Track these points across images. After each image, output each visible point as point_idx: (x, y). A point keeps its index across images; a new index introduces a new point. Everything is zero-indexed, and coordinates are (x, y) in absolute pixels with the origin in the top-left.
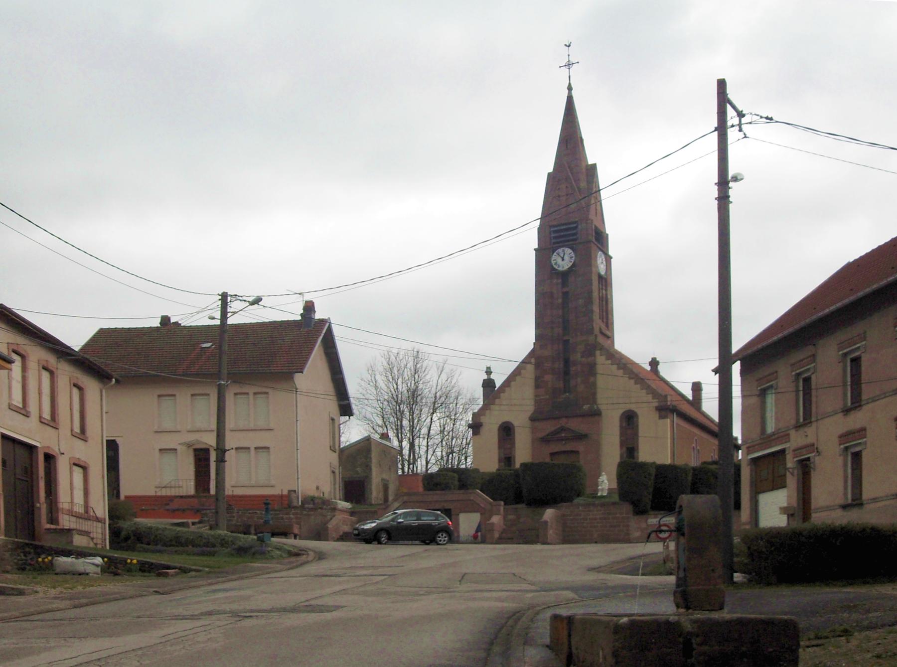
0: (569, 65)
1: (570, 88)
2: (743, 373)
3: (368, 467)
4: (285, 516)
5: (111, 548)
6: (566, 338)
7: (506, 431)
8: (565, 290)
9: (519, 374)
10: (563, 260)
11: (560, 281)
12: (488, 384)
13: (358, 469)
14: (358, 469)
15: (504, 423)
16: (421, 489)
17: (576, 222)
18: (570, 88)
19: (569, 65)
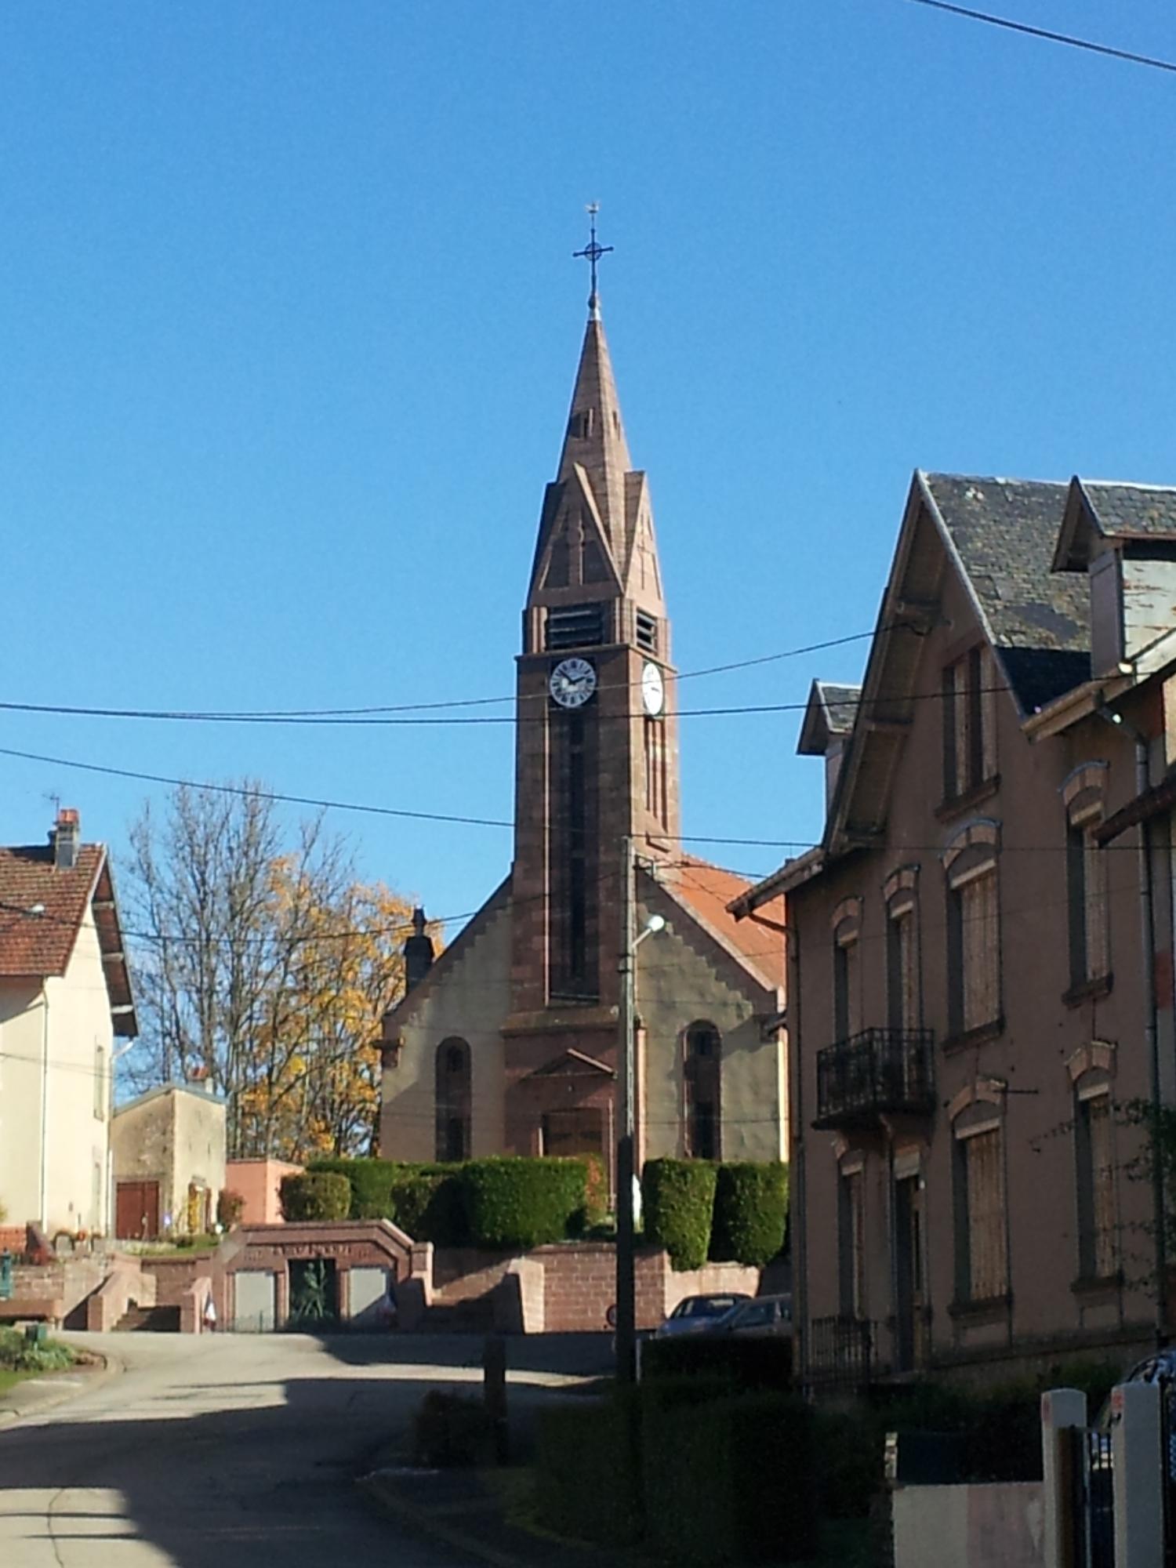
0: (593, 252)
1: (584, 429)
2: (439, 1396)
3: (166, 1151)
4: (35, 1282)
5: (788, 1289)
6: (576, 855)
7: (452, 1060)
8: (577, 749)
9: (482, 931)
10: (572, 687)
11: (566, 728)
12: (418, 948)
13: (144, 1157)
14: (144, 1157)
15: (439, 1048)
16: (279, 1220)
17: (597, 605)
18: (584, 429)
19: (593, 252)
